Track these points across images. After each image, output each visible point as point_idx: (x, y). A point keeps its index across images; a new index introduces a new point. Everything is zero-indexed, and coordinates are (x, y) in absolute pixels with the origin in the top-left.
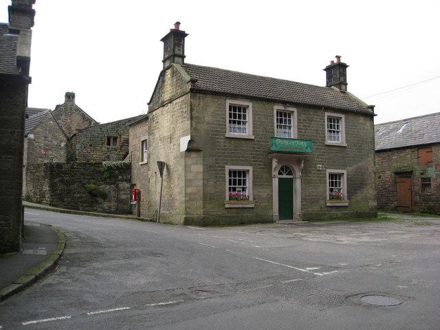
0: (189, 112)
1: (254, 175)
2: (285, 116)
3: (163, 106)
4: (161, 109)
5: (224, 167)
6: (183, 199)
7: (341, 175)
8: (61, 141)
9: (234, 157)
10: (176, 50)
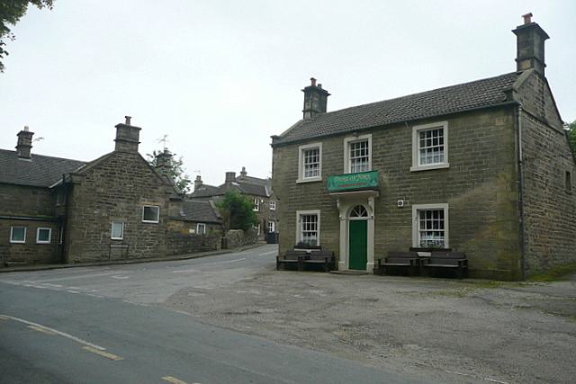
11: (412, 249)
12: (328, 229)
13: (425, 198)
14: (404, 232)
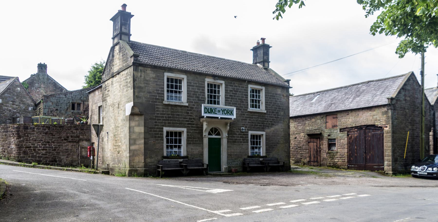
0: (132, 82)
1: (187, 135)
2: (256, 93)
3: (113, 77)
4: (111, 80)
5: (163, 129)
6: (128, 155)
7: (260, 136)
8: (29, 106)
9: (171, 120)
10: (123, 29)
11: (249, 157)
12: (194, 143)
13: (255, 128)
14: (244, 147)
